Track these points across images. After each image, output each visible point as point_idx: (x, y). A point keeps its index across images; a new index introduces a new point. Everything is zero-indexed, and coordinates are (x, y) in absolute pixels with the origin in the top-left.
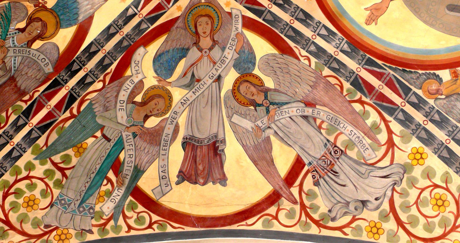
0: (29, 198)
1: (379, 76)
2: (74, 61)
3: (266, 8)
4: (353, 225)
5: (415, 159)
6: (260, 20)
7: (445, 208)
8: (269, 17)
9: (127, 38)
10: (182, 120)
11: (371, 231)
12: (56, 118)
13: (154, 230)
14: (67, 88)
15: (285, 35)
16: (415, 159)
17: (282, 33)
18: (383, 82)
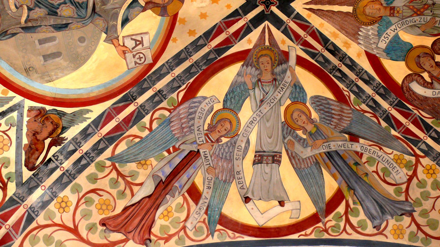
0: (58, 202)
1: (406, 115)
2: (145, 80)
3: (320, 52)
4: (344, 218)
5: (63, 201)
6: (313, 61)
7: (432, 210)
8: (321, 59)
9: (177, 79)
10: (253, 138)
11: (60, 203)
12: (233, 45)
13: (387, 237)
14: (155, 90)
15: (333, 76)
16: (63, 201)
17: (331, 73)
18: (409, 121)
